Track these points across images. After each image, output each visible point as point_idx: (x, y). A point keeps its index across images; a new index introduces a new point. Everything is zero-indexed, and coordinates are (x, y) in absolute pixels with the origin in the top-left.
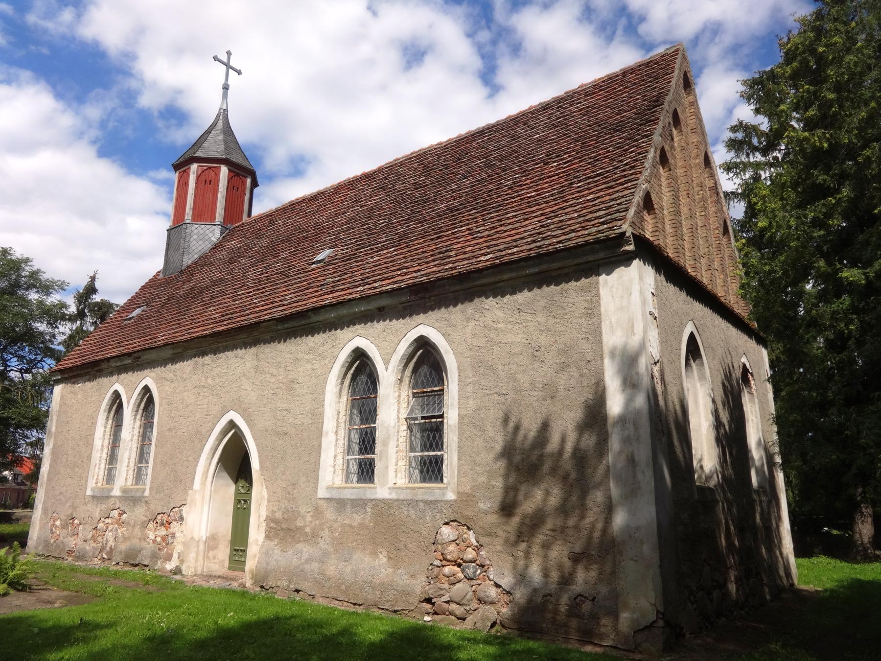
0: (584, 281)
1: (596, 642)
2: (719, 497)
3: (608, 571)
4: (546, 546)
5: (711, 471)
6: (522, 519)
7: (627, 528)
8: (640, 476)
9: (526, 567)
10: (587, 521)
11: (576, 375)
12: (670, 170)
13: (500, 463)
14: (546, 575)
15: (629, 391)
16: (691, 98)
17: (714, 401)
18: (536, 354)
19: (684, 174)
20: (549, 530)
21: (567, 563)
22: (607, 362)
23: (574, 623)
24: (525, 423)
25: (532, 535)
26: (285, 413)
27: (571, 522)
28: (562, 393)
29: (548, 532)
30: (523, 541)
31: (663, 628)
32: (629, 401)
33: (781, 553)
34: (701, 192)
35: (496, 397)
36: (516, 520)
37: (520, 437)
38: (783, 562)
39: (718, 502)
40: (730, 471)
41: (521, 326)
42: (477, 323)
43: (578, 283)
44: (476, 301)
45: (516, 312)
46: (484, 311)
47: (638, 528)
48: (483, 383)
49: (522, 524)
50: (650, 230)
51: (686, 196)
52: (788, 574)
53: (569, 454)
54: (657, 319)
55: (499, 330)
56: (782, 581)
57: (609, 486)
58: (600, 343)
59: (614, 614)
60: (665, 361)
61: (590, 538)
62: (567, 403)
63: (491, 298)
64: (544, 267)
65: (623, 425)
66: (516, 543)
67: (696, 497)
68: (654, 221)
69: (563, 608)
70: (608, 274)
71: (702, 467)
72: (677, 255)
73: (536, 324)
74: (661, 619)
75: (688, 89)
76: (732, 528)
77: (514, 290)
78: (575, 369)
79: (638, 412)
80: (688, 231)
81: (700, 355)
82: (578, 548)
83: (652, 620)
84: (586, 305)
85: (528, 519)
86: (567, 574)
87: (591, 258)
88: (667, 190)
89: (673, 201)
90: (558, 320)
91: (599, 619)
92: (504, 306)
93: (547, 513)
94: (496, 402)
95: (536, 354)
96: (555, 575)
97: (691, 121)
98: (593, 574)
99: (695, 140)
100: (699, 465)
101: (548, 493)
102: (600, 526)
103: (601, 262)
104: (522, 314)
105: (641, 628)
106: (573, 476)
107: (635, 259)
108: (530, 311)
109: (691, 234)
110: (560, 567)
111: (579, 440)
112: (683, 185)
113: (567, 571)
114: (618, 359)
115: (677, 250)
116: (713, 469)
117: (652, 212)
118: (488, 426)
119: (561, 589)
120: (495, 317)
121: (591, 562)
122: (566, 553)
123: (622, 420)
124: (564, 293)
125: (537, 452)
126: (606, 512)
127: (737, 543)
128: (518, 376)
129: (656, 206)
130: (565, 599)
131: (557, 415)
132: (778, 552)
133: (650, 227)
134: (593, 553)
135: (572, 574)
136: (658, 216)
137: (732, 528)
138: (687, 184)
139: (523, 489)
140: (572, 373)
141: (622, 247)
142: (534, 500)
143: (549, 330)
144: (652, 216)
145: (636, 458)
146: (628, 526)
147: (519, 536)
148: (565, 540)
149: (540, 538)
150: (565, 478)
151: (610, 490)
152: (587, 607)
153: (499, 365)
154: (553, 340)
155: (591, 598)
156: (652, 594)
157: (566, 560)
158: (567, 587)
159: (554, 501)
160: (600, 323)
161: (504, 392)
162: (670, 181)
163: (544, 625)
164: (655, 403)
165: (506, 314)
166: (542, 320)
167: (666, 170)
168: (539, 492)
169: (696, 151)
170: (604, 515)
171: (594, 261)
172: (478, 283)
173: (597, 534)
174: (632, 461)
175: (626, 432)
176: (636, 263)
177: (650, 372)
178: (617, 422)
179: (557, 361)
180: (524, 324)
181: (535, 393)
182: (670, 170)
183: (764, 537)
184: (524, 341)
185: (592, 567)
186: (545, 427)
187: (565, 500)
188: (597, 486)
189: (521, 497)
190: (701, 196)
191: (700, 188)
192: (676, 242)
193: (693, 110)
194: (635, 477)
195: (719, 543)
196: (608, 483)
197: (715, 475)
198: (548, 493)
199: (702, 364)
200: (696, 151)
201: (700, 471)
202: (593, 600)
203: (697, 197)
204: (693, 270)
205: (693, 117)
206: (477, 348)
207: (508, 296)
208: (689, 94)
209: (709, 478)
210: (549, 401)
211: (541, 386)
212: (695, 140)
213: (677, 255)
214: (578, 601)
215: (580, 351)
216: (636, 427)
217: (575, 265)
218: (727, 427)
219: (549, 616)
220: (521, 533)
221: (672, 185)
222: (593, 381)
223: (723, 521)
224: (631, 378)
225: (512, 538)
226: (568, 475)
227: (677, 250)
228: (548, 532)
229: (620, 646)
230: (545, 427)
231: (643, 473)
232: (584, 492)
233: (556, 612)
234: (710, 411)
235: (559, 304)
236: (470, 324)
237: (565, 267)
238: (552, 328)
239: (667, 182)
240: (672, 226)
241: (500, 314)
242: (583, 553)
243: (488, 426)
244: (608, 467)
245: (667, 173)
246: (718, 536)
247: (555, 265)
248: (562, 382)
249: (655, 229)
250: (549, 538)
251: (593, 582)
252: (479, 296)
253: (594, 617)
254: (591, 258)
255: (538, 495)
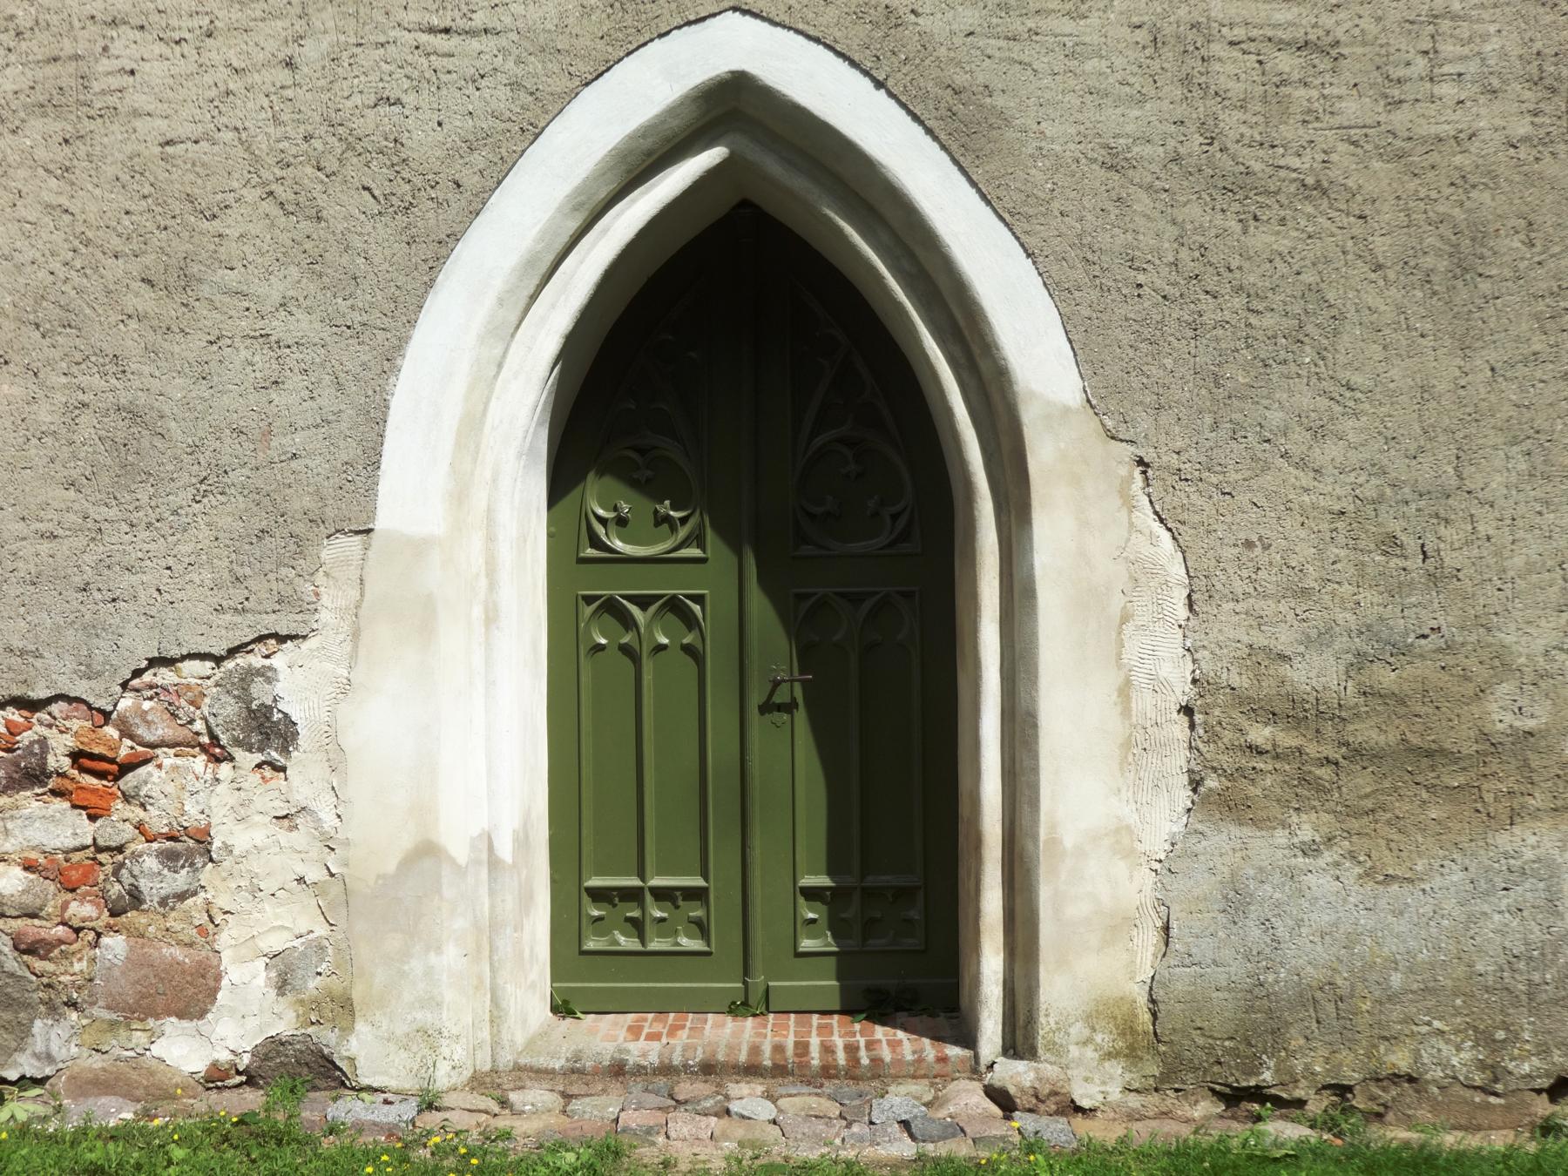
26: (1286, 62)
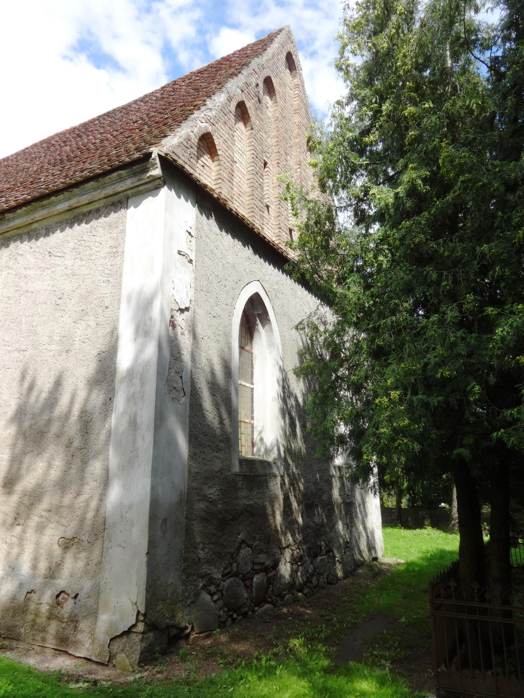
0: (113, 216)
1: (70, 652)
2: (278, 470)
3: (95, 562)
4: (40, 529)
5: (271, 444)
6: (20, 498)
7: (120, 505)
8: (139, 443)
9: (19, 555)
10: (83, 498)
11: (93, 324)
12: (252, 129)
13: (9, 431)
14: (34, 567)
15: (140, 340)
16: (296, 81)
17: (282, 370)
18: (59, 302)
19: (276, 144)
20: (44, 510)
21: (57, 551)
22: (123, 306)
23: (53, 627)
24: (39, 383)
25: (28, 517)
27: (67, 500)
28: (77, 345)
29: (43, 513)
30: (18, 525)
31: (143, 633)
32: (140, 351)
33: (365, 528)
34: (299, 170)
35: (16, 354)
36: (15, 498)
37: (32, 399)
38: (368, 537)
39: (275, 476)
40: (299, 444)
41: (49, 271)
42: (10, 271)
43: (107, 219)
44: (12, 245)
45: (47, 256)
46: (18, 257)
47: (130, 506)
48: (6, 339)
49: (20, 503)
50: (214, 178)
51: (276, 165)
52: (371, 547)
53: (75, 418)
54: (194, 262)
55: (29, 278)
56: (362, 556)
57: (108, 455)
58: (119, 285)
59: (94, 614)
60: (200, 312)
61: (82, 520)
62: (80, 357)
63: (26, 243)
64: (73, 202)
65: (130, 380)
66: (12, 525)
67: (236, 469)
68: (218, 168)
69: (44, 609)
70: (136, 207)
71: (262, 439)
72: (251, 214)
73: (63, 268)
74: (142, 621)
75: (294, 72)
76: (295, 505)
77: (48, 231)
78: (92, 318)
79: (147, 364)
80: (275, 200)
81: (269, 320)
82: (69, 534)
83: (130, 624)
84: (112, 243)
85: (26, 497)
86: (54, 566)
87: (120, 187)
88: (248, 149)
89: (253, 160)
90: (83, 263)
91: (77, 621)
92: (37, 250)
93: (46, 490)
94: (15, 360)
95: (59, 302)
96: (43, 566)
97: (295, 103)
98: (80, 564)
99: (297, 121)
100: (259, 437)
101: (50, 466)
102: (94, 504)
103: (129, 192)
104: (52, 257)
105: (118, 634)
106: (77, 443)
107: (163, 186)
108: (60, 255)
109: (278, 203)
110: (50, 555)
111: (87, 400)
112: (274, 155)
113: (55, 560)
114: (134, 302)
115: (251, 210)
116: (274, 442)
117: (216, 158)
118: (4, 388)
119: (46, 584)
120: (27, 263)
121: (80, 550)
122: (57, 538)
123: (131, 373)
124: (93, 231)
125: (45, 417)
126: (102, 487)
127: (300, 520)
128: (39, 329)
129: (219, 152)
130: (47, 597)
131: (69, 372)
132: (361, 528)
133: (214, 174)
134: (83, 538)
135: (59, 565)
136: (222, 163)
137: (295, 505)
138: (278, 154)
139: (27, 460)
140: (89, 323)
141: (148, 172)
142: (35, 474)
143: (74, 275)
144: (216, 163)
145: (139, 420)
146: (121, 503)
147: (16, 519)
148: (58, 522)
149: (34, 520)
150: (69, 444)
151: (108, 459)
152: (69, 606)
153: (24, 317)
154: (76, 285)
155: (73, 596)
156: (134, 590)
157: (56, 547)
158: (52, 581)
159: (55, 474)
160: (122, 264)
161: (24, 348)
162: (251, 140)
163: (22, 630)
164: (172, 355)
165: (37, 258)
166: (69, 263)
167: (248, 128)
168: (41, 464)
169: (297, 130)
170: (99, 491)
171: (123, 191)
172: (12, 224)
173: (90, 515)
174: (133, 424)
175: (132, 389)
176: (165, 191)
177: (168, 318)
178: (125, 377)
179: (77, 310)
180: (53, 269)
181: (53, 347)
182: (252, 129)
183: (344, 513)
184: (50, 288)
185: (80, 555)
186: (58, 384)
187: (66, 472)
188: (95, 456)
189: (23, 471)
190: (298, 174)
191: (298, 166)
192: (252, 202)
193: (297, 92)
194: (134, 442)
195: (271, 521)
196: (108, 450)
197: (275, 449)
198: (50, 466)
199: (271, 330)
200: (297, 130)
201: (259, 445)
202: (76, 597)
203: (295, 174)
204: (277, 238)
205: (297, 98)
206: (6, 299)
207: (42, 239)
208: (294, 77)
209: (267, 451)
210: (64, 355)
211: (58, 338)
212: (297, 121)
213: (251, 214)
214: (60, 598)
215: (99, 295)
216: (143, 382)
217: (106, 198)
218: (300, 400)
219: (30, 617)
220: (18, 514)
221: (253, 143)
222: (109, 330)
223: (281, 497)
224: (145, 324)
225: (10, 520)
226: (71, 443)
227: (251, 210)
228: (43, 513)
229: (93, 658)
230: (58, 384)
231: (143, 438)
232: (85, 462)
233: (37, 614)
234: (276, 380)
235: (87, 244)
236: (3, 273)
237: (95, 201)
238: (77, 272)
239: (248, 141)
240: (249, 185)
241: (31, 258)
242: (74, 538)
243: (4, 388)
244: (110, 431)
245: (249, 132)
246: (269, 511)
247: (85, 199)
248: (79, 333)
249: (218, 176)
250: (44, 520)
251: (79, 574)
252: (15, 241)
253: (74, 620)
254: (120, 187)
255: (40, 466)
